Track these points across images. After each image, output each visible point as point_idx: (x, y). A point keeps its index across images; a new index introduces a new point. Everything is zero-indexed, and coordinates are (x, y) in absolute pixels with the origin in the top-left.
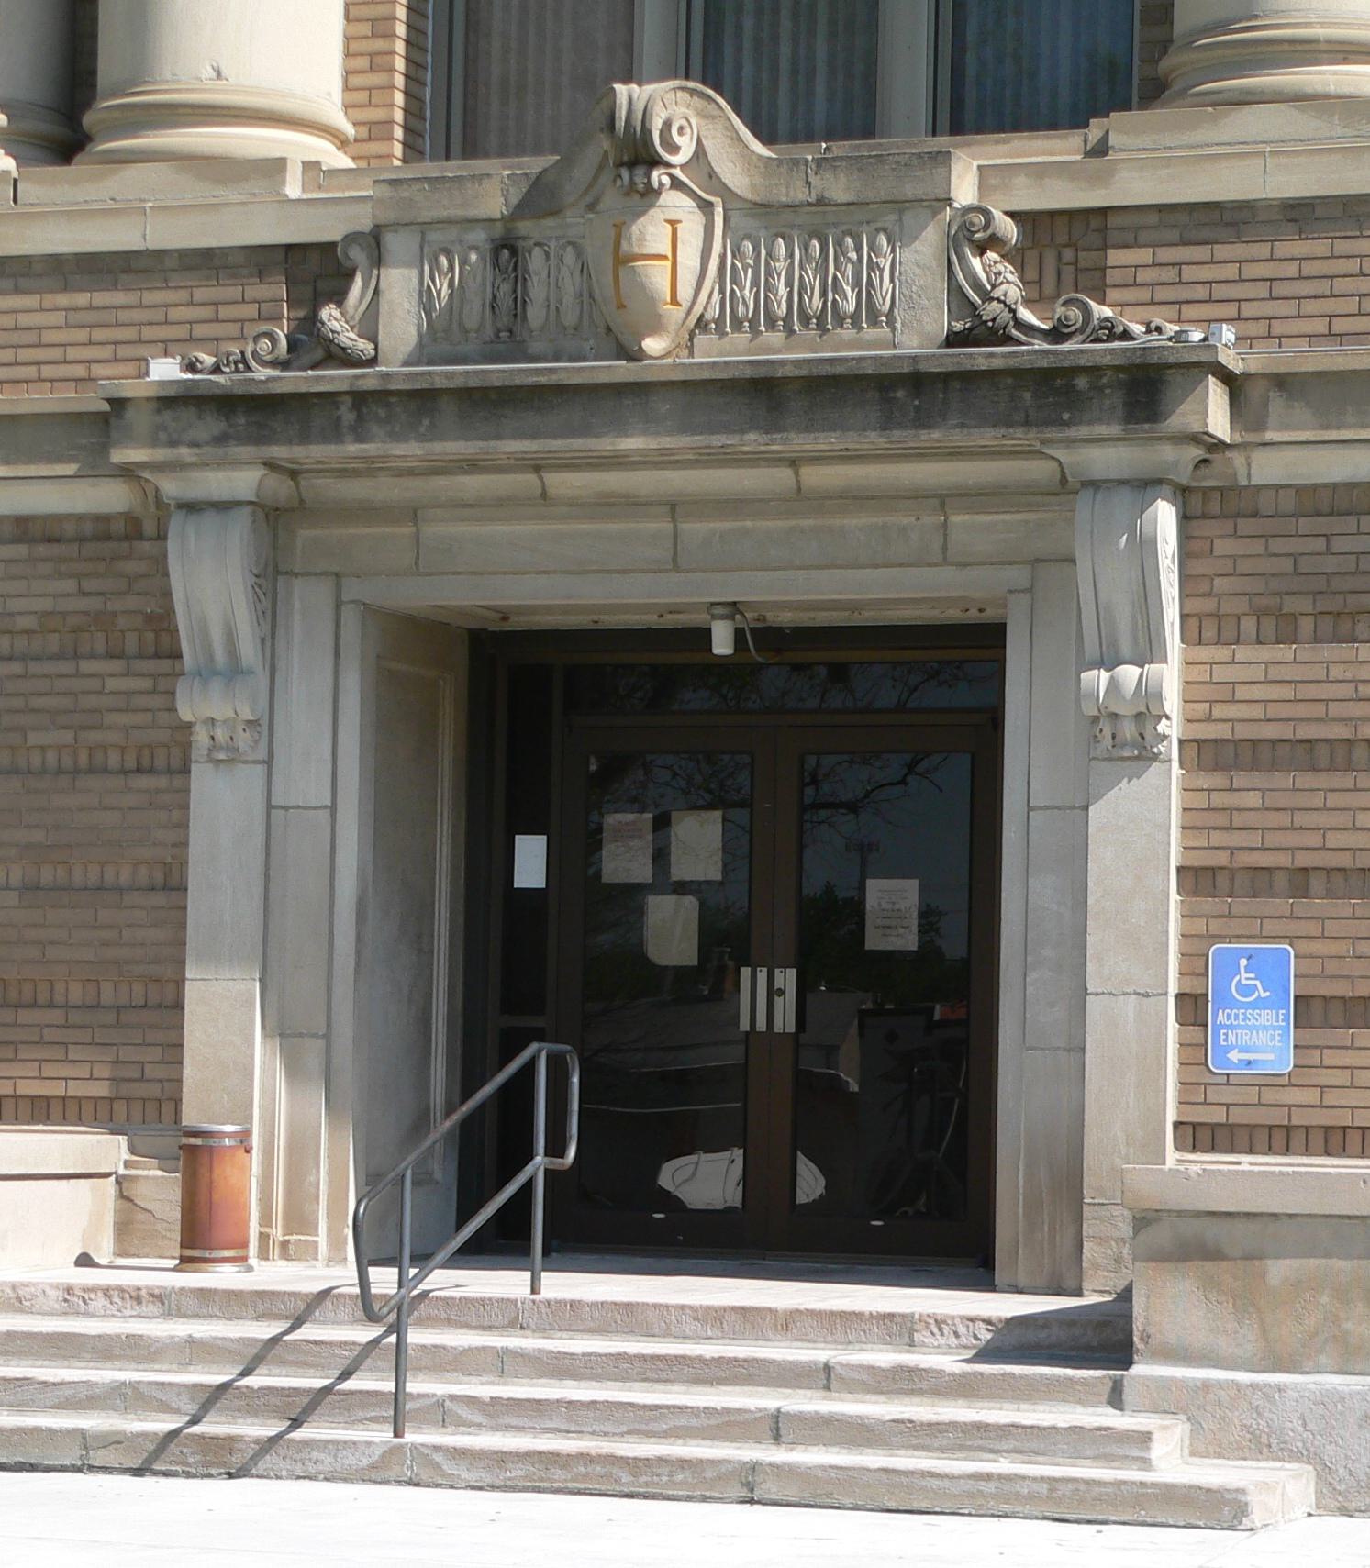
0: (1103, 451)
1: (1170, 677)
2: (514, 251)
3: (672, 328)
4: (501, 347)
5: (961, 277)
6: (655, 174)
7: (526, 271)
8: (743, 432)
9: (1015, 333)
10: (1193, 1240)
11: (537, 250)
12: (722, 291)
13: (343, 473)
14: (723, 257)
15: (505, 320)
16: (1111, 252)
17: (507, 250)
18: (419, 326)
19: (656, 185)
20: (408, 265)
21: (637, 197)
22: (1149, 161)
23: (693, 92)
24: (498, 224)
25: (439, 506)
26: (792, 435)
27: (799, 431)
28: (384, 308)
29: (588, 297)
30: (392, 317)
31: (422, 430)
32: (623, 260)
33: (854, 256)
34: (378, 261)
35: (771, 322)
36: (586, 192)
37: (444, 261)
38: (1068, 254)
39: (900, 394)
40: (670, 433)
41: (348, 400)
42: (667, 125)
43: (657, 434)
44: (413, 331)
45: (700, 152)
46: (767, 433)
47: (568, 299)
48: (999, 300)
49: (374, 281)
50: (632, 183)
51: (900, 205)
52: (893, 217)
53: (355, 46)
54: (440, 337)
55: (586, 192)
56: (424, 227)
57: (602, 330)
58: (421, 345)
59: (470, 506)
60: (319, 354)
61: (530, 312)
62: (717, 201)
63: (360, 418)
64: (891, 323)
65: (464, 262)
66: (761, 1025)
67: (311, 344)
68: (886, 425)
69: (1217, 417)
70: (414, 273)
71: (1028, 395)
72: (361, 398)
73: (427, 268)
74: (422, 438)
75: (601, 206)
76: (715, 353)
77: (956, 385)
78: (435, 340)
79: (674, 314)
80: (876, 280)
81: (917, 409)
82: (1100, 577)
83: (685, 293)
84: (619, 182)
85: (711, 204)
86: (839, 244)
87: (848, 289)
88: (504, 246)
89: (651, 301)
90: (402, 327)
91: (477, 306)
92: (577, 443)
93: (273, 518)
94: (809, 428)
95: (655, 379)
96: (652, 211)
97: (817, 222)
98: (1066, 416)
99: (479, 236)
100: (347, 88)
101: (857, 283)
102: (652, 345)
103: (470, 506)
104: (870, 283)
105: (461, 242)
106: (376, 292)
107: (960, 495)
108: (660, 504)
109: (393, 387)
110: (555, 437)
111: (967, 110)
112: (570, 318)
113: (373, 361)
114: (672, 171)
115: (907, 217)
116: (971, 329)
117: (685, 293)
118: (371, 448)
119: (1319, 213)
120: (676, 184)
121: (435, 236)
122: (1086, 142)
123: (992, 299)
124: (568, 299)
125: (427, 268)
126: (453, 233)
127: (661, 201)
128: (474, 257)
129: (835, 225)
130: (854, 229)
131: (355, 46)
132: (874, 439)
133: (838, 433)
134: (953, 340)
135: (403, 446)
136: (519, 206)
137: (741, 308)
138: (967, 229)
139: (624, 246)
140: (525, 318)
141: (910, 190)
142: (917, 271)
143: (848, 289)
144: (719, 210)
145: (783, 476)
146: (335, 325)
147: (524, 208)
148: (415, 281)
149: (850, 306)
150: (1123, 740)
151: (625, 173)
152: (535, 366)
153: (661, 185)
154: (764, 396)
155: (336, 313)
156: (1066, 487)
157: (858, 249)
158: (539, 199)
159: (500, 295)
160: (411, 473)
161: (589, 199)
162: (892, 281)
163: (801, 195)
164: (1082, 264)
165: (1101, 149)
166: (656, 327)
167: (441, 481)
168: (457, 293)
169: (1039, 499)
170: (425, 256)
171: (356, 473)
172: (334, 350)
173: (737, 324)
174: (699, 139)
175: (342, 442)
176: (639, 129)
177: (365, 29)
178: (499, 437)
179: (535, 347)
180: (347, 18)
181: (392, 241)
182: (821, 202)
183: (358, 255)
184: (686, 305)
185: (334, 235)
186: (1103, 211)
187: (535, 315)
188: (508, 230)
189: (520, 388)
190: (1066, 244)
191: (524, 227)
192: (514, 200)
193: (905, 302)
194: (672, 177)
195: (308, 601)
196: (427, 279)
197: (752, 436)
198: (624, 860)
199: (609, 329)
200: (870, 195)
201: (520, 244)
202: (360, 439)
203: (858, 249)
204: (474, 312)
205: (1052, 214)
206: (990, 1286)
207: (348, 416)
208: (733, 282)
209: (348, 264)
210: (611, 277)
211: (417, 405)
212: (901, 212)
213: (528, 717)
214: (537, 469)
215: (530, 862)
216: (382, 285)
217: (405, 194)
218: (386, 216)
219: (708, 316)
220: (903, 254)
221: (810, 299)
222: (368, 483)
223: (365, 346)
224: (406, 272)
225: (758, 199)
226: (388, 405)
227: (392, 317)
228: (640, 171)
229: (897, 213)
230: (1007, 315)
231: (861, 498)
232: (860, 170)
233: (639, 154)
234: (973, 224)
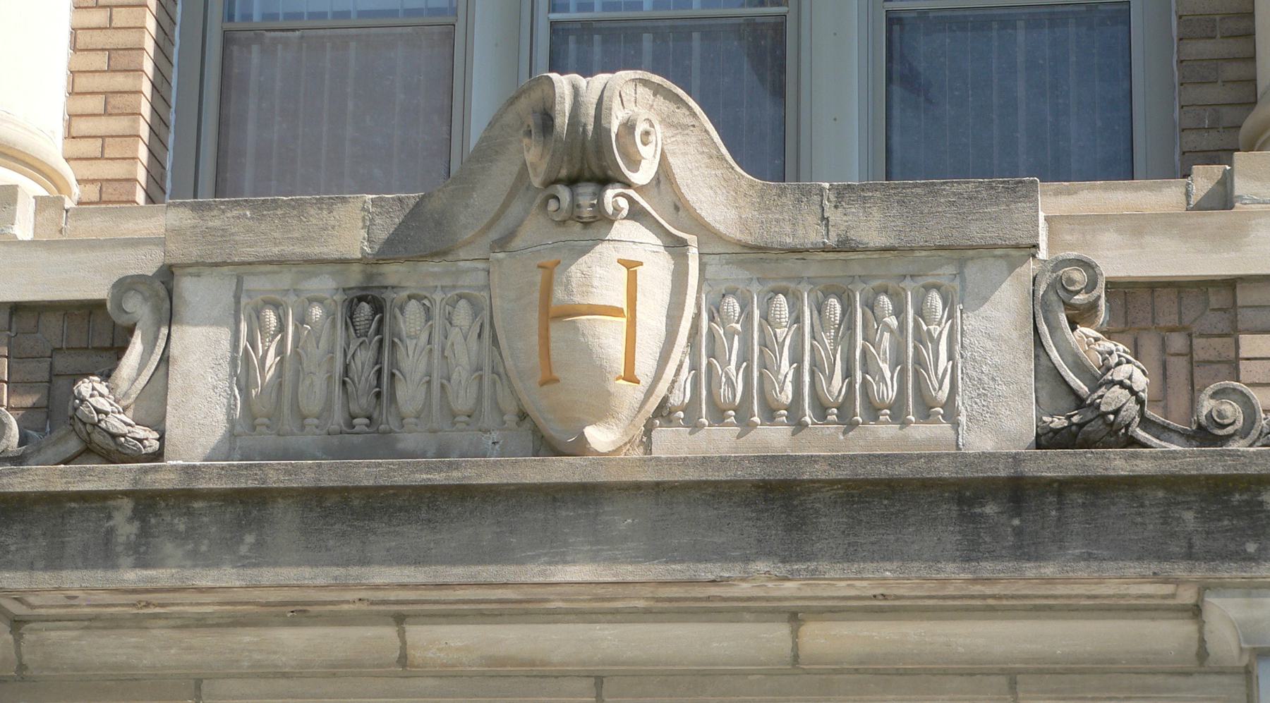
2: (378, 307)
3: (625, 413)
4: (357, 439)
5: (1054, 355)
6: (610, 193)
7: (396, 334)
8: (747, 559)
9: (1141, 434)
11: (413, 305)
12: (694, 367)
13: (93, 623)
14: (697, 317)
15: (363, 402)
16: (1245, 339)
17: (367, 306)
18: (230, 409)
19: (610, 210)
20: (217, 323)
21: (578, 227)
23: (657, 90)
24: (356, 268)
25: (241, 676)
26: (824, 566)
27: (833, 559)
28: (175, 382)
29: (494, 371)
31: (243, 550)
32: (556, 314)
33: (893, 321)
34: (169, 316)
35: (770, 414)
36: (489, 227)
37: (271, 318)
38: (1177, 342)
39: (990, 509)
40: (633, 560)
41: (127, 505)
42: (629, 126)
43: (614, 560)
44: (221, 415)
45: (664, 174)
46: (784, 561)
47: (461, 372)
48: (1121, 384)
49: (161, 344)
50: (575, 205)
51: (960, 253)
52: (950, 270)
53: (84, 83)
54: (254, 424)
55: (489, 227)
56: (242, 269)
57: (511, 418)
58: (232, 435)
59: (285, 675)
60: (73, 445)
61: (402, 392)
62: (691, 239)
63: (145, 533)
64: (951, 414)
65: (301, 320)
68: (970, 553)
70: (225, 335)
71: (1189, 516)
72: (147, 503)
73: (244, 327)
74: (243, 563)
75: (517, 243)
77: (1078, 498)
78: (254, 428)
79: (628, 396)
80: (927, 355)
81: (1018, 532)
83: (645, 365)
84: (552, 205)
85: (683, 243)
86: (870, 305)
87: (885, 368)
88: (360, 299)
89: (599, 371)
91: (319, 380)
92: (488, 572)
94: (850, 555)
95: (612, 478)
96: (599, 248)
97: (838, 274)
98: (1251, 547)
99: (324, 284)
100: (70, 136)
101: (898, 360)
102: (600, 437)
103: (285, 675)
104: (919, 361)
105: (297, 292)
106: (165, 360)
107: (1040, 672)
108: (579, 676)
109: (202, 485)
110: (453, 561)
112: (463, 401)
113: (158, 455)
114: (631, 192)
115: (971, 270)
116: (1080, 426)
117: (645, 365)
118: (162, 576)
120: (637, 213)
121: (258, 284)
122: (1188, 195)
123: (1112, 383)
124: (461, 372)
125: (244, 327)
126: (285, 279)
127: (613, 234)
128: (317, 312)
129: (863, 279)
130: (892, 284)
131: (84, 83)
132: (955, 577)
133: (895, 565)
134: (1047, 440)
135: (214, 573)
136: (390, 242)
137: (724, 391)
138: (1061, 287)
139: (559, 294)
140: (393, 398)
141: (977, 231)
142: (989, 344)
143: (885, 368)
144: (693, 252)
145: (776, 635)
146: (103, 404)
147: (397, 247)
148: (226, 345)
149: (889, 392)
151: (564, 193)
153: (617, 210)
154: (780, 508)
155: (102, 388)
157: (899, 312)
158: (419, 237)
159: (356, 367)
160: (201, 623)
161: (494, 235)
162: (951, 357)
163: (813, 234)
164: (1199, 355)
165: (1223, 198)
166: (602, 414)
167: (246, 637)
168: (292, 365)
169: (1160, 679)
170: (243, 309)
171: (114, 623)
172: (97, 437)
173: (718, 415)
174: (663, 155)
175: (115, 567)
176: (590, 128)
177: (100, 61)
178: (364, 562)
179: (408, 441)
180: (75, 48)
181: (188, 287)
182: (845, 246)
183: (138, 308)
184: (645, 381)
185: (98, 290)
186: (1231, 283)
187: (409, 394)
188: (370, 277)
189: (399, 490)
191: (393, 273)
192: (383, 235)
194: (631, 201)
196: (243, 342)
197: (761, 566)
199: (523, 416)
200: (919, 238)
201: (388, 295)
202: (142, 564)
203: (899, 312)
204: (316, 390)
205: (1153, 286)
207: (125, 529)
208: (711, 354)
209: (122, 320)
210: (535, 339)
211: (235, 512)
212: (962, 264)
214: (399, 620)
216: (175, 350)
217: (217, 223)
218: (179, 252)
219: (676, 400)
220: (972, 322)
221: (830, 379)
222: (132, 638)
223: (151, 439)
224: (212, 331)
225: (750, 240)
226: (190, 513)
228: (586, 193)
230: (1132, 408)
231: (886, 673)
232: (901, 203)
233: (588, 165)
234: (1071, 281)
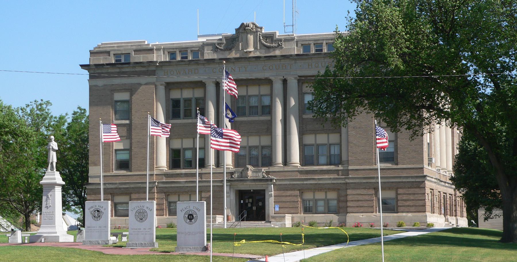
0: (270, 183)
1: (273, 193)
10: (273, 217)
17: (241, 173)
22: (271, 169)
30: (236, 176)
66: (112, 129)
67: (232, 177)
69: (274, 181)
76: (252, 178)
82: (269, 188)
90: (236, 176)
93: (230, 185)
111: (263, 165)
119: (216, 61)
150: (271, 195)
152: (243, 178)
154: (254, 180)
156: (268, 184)
158: (243, 170)
190: (268, 173)
193: (260, 176)
195: (232, 189)
198: (247, 201)
206: (131, 171)
213: (241, 194)
215: (242, 202)
227: (236, 176)
229: (260, 171)
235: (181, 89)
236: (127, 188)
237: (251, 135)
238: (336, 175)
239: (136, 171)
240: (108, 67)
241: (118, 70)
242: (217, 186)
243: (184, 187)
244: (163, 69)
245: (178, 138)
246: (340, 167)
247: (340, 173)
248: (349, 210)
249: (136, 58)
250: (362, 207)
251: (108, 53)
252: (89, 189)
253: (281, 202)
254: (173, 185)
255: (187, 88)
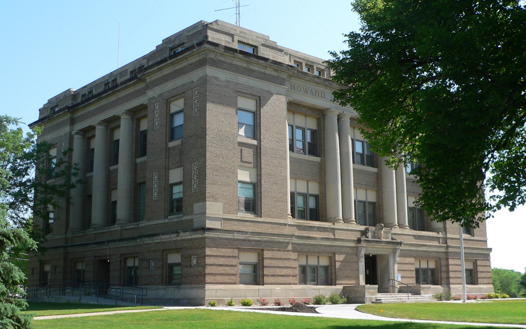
17: (374, 232)
235: (294, 113)
236: (259, 241)
237: (361, 188)
238: (437, 242)
239: (269, 216)
240: (240, 56)
241: (244, 65)
242: (349, 247)
243: (317, 245)
244: (291, 80)
245: (168, 173)
246: (441, 235)
247: (441, 240)
248: (208, 279)
249: (263, 52)
250: (289, 267)
251: (232, 36)
252: (209, 238)
253: (404, 270)
254: (276, 238)
255: (300, 113)
